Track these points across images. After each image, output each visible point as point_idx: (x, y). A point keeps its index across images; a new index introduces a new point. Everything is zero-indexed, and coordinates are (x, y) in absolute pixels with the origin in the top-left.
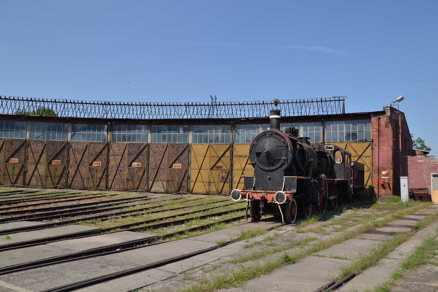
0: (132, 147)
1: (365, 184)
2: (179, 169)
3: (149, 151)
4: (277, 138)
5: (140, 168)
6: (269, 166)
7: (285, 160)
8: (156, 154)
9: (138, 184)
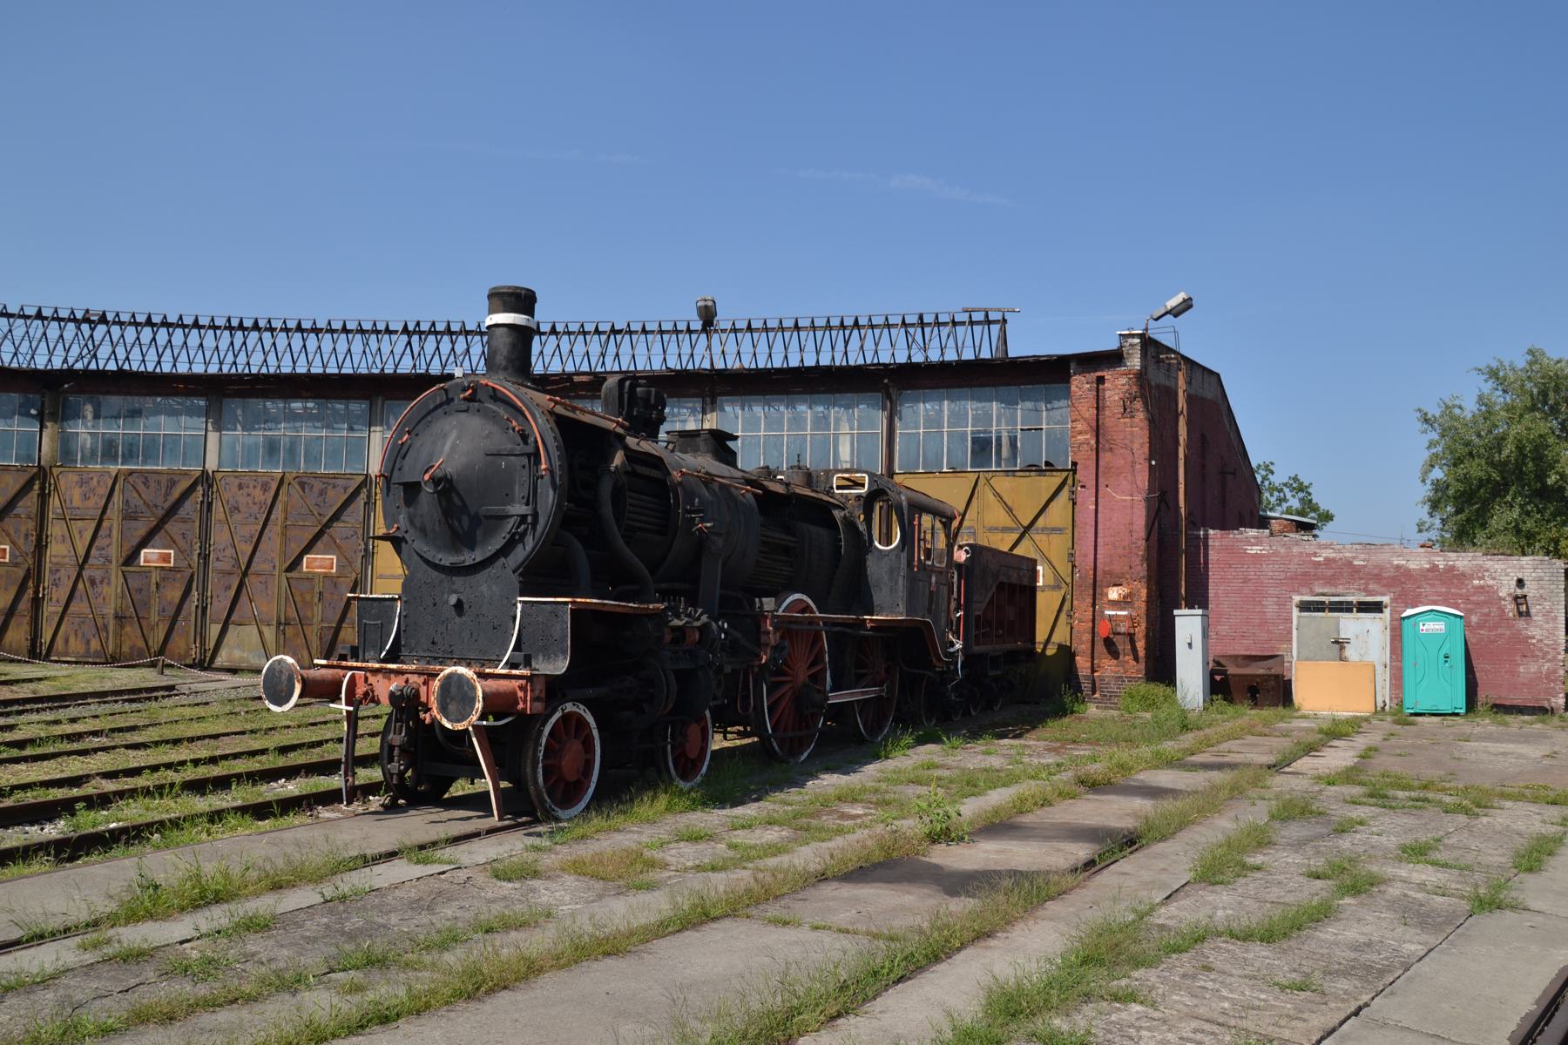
0: (141, 487)
1: (1041, 636)
2: (326, 576)
3: (210, 505)
4: (494, 417)
5: (170, 569)
6: (457, 551)
7: (523, 518)
8: (237, 517)
9: (161, 637)
